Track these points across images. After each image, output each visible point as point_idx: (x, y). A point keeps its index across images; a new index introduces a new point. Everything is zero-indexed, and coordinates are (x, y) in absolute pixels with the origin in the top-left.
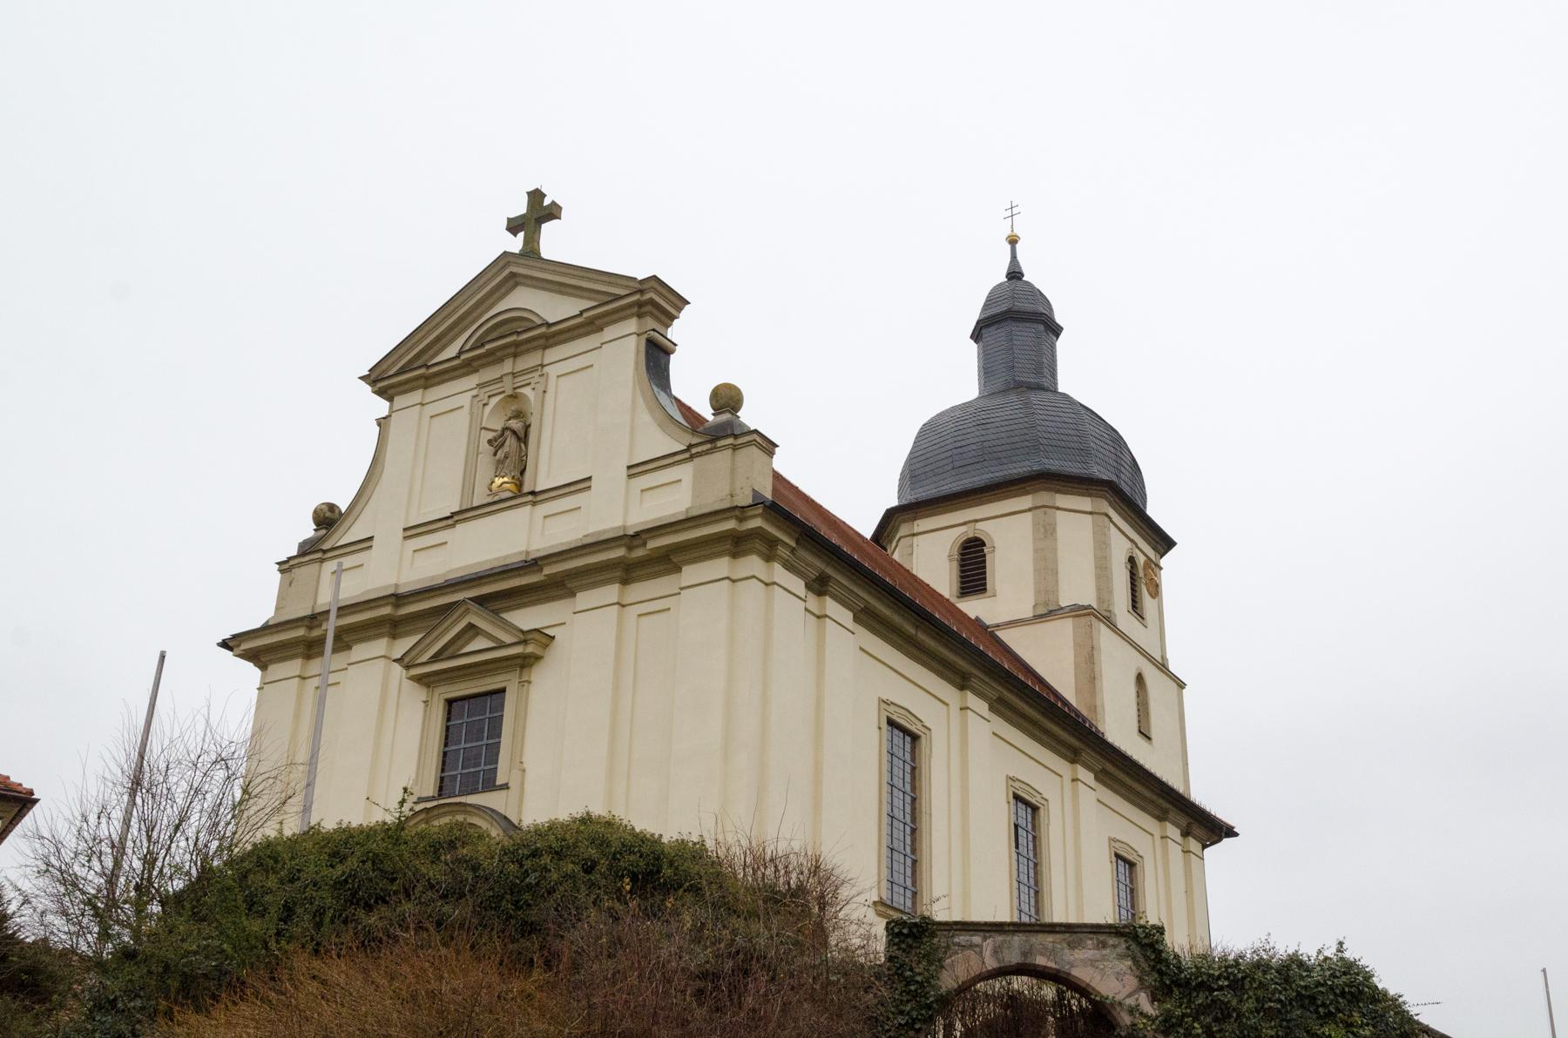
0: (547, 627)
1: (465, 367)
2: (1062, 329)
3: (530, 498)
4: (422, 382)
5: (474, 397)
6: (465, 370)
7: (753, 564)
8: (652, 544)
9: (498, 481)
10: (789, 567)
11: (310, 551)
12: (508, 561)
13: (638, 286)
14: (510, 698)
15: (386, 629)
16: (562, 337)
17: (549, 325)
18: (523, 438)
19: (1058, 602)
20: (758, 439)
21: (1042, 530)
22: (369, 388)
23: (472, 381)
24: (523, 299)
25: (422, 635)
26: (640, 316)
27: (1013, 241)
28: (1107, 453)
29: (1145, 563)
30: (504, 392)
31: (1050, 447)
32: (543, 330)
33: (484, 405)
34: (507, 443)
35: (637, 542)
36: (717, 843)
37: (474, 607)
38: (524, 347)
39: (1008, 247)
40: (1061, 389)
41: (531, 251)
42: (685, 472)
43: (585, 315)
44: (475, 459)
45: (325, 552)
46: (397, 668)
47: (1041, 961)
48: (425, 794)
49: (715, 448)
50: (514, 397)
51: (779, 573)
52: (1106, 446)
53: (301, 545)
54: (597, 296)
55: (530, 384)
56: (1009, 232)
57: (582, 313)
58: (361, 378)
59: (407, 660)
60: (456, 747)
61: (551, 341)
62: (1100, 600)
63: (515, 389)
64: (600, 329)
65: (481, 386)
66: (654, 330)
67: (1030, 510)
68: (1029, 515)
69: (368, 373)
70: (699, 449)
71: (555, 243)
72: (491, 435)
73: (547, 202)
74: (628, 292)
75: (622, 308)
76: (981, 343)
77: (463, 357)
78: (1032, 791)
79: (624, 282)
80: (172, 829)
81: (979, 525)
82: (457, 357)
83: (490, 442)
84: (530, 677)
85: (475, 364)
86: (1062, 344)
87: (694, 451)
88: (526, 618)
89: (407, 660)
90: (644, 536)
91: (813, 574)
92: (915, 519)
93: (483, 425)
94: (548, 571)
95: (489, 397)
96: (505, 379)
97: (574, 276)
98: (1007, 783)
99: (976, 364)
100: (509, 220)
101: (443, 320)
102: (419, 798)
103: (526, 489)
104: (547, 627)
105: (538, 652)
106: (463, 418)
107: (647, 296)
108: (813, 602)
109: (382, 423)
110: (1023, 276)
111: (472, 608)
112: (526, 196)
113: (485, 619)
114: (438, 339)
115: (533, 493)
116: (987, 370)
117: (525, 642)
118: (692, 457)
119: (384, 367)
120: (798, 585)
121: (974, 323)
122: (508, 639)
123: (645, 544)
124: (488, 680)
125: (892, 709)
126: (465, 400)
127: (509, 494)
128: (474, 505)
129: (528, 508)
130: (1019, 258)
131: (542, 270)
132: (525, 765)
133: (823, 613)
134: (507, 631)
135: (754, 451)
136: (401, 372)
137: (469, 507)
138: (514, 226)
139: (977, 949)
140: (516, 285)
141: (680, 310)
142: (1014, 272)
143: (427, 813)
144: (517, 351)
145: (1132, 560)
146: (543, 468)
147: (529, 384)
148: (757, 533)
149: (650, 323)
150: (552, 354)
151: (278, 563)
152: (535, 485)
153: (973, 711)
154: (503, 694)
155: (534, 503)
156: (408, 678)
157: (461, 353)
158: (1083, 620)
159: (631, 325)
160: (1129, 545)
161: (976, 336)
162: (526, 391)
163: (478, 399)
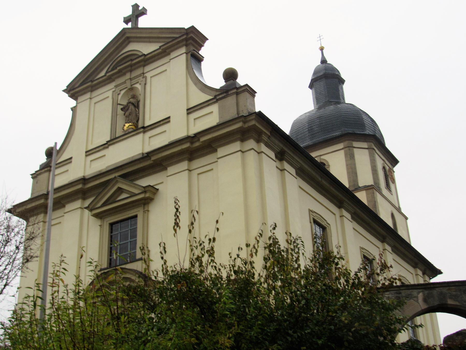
0: (156, 185)
1: (108, 80)
3: (142, 130)
4: (90, 89)
6: (108, 81)
7: (251, 144)
8: (203, 139)
9: (127, 125)
10: (267, 145)
11: (46, 167)
14: (140, 220)
15: (80, 196)
17: (145, 55)
18: (137, 106)
19: (358, 185)
20: (248, 89)
21: (349, 156)
22: (67, 95)
23: (112, 85)
24: (133, 47)
27: (322, 49)
28: (370, 126)
29: (389, 169)
32: (142, 58)
33: (119, 94)
34: (130, 108)
35: (196, 139)
37: (120, 180)
39: (320, 52)
40: (347, 102)
41: (135, 27)
43: (162, 48)
44: (116, 117)
46: (86, 211)
47: (450, 302)
48: (103, 267)
49: (229, 95)
50: (132, 89)
51: (264, 148)
52: (369, 123)
53: (41, 166)
54: (161, 40)
56: (320, 46)
57: (160, 47)
58: (64, 91)
59: (91, 207)
60: (116, 233)
61: (147, 62)
62: (375, 182)
63: (132, 85)
64: (169, 54)
65: (116, 86)
66: (194, 50)
69: (66, 88)
70: (221, 96)
71: (143, 22)
72: (122, 107)
73: (140, 8)
74: (180, 35)
75: (179, 42)
76: (313, 89)
77: (108, 75)
78: (370, 254)
81: (322, 157)
82: (105, 75)
83: (122, 109)
84: (148, 208)
85: (113, 78)
86: (345, 87)
87: (218, 97)
88: (145, 182)
89: (91, 207)
90: (198, 136)
91: (278, 150)
93: (119, 103)
94: (153, 158)
95: (120, 91)
96: (127, 82)
98: (360, 250)
99: (312, 97)
100: (124, 18)
103: (140, 125)
104: (156, 185)
105: (151, 196)
106: (110, 101)
107: (190, 36)
108: (278, 164)
109: (74, 109)
110: (327, 62)
111: (118, 180)
112: (131, 8)
113: (126, 184)
114: (96, 69)
115: (143, 127)
116: (317, 99)
117: (145, 192)
118: (217, 100)
119: (73, 84)
120: (272, 155)
121: (310, 81)
122: (136, 191)
123: (199, 140)
124: (128, 212)
125: (314, 214)
126: (110, 94)
127: (131, 130)
128: (117, 136)
130: (325, 55)
131: (141, 33)
133: (283, 168)
134: (136, 188)
135: (247, 94)
137: (114, 137)
138: (127, 21)
139: (415, 299)
140: (129, 42)
141: (204, 42)
144: (131, 68)
145: (384, 168)
146: (147, 116)
148: (254, 128)
149: (192, 48)
150: (147, 68)
151: (31, 175)
152: (144, 124)
153: (345, 217)
154: (136, 218)
155: (144, 132)
156: (92, 216)
157: (107, 72)
158: (370, 191)
159: (183, 50)
160: (382, 162)
161: (311, 86)
162: (138, 86)
163: (115, 92)
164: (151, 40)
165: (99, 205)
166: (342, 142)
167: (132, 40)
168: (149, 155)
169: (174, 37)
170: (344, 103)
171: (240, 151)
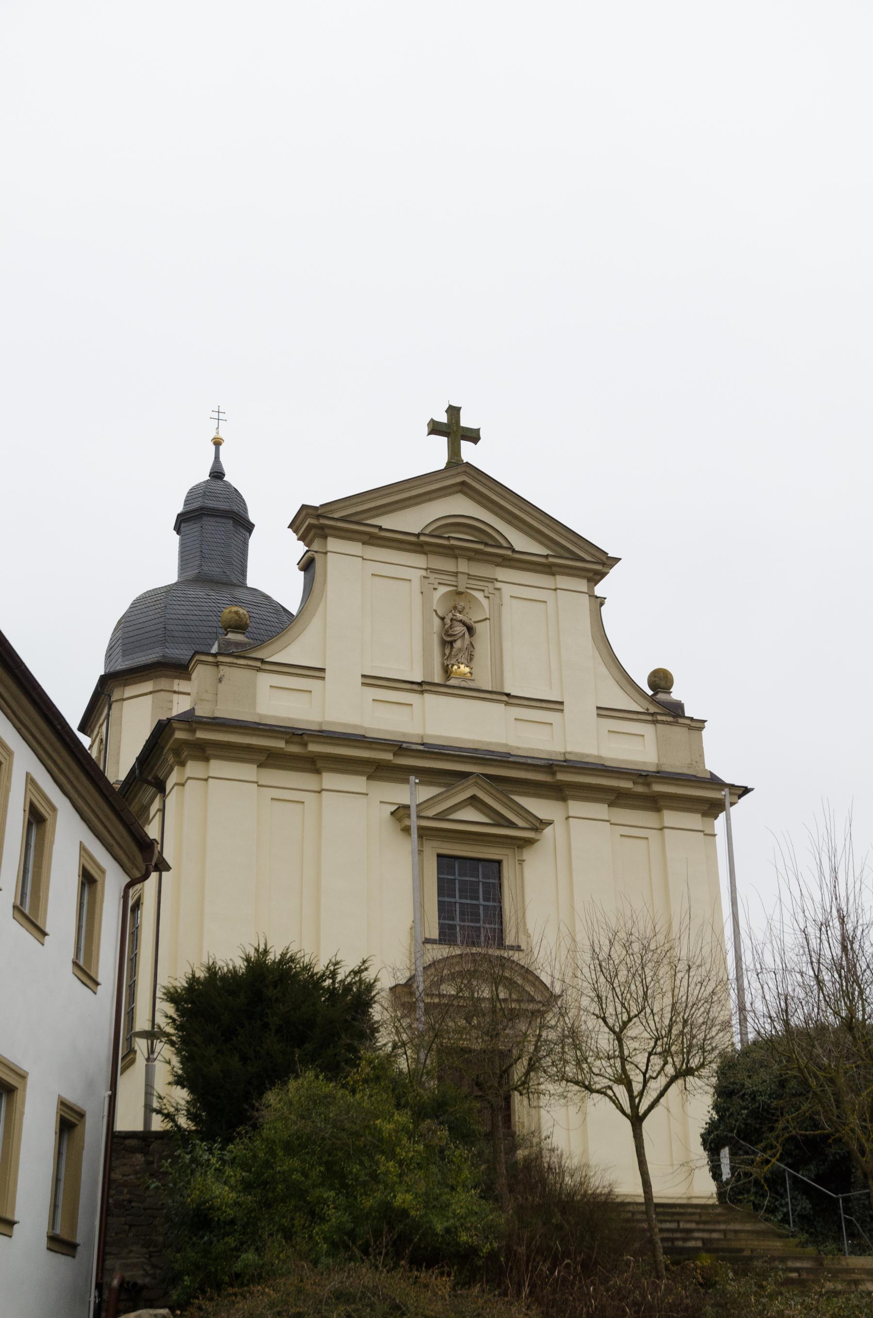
0: (728, 819)
2: (253, 526)
5: (425, 577)
13: (604, 559)
16: (517, 564)
17: (514, 551)
23: (419, 560)
27: (217, 443)
30: (456, 586)
31: (180, 639)
38: (375, 541)
39: (213, 447)
42: (648, 730)
45: (263, 661)
54: (553, 546)
55: (483, 591)
57: (547, 556)
67: (151, 693)
68: (150, 696)
77: (422, 538)
79: (593, 551)
80: (809, 965)
85: (426, 548)
92: (125, 685)
110: (224, 475)
118: (655, 722)
119: (333, 507)
124: (484, 849)
129: (502, 706)
130: (222, 459)
136: (342, 519)
142: (216, 472)
144: (475, 556)
150: (502, 573)
161: (183, 522)
163: (428, 581)
164: (515, 522)
166: (151, 679)
169: (580, 556)
170: (242, 585)
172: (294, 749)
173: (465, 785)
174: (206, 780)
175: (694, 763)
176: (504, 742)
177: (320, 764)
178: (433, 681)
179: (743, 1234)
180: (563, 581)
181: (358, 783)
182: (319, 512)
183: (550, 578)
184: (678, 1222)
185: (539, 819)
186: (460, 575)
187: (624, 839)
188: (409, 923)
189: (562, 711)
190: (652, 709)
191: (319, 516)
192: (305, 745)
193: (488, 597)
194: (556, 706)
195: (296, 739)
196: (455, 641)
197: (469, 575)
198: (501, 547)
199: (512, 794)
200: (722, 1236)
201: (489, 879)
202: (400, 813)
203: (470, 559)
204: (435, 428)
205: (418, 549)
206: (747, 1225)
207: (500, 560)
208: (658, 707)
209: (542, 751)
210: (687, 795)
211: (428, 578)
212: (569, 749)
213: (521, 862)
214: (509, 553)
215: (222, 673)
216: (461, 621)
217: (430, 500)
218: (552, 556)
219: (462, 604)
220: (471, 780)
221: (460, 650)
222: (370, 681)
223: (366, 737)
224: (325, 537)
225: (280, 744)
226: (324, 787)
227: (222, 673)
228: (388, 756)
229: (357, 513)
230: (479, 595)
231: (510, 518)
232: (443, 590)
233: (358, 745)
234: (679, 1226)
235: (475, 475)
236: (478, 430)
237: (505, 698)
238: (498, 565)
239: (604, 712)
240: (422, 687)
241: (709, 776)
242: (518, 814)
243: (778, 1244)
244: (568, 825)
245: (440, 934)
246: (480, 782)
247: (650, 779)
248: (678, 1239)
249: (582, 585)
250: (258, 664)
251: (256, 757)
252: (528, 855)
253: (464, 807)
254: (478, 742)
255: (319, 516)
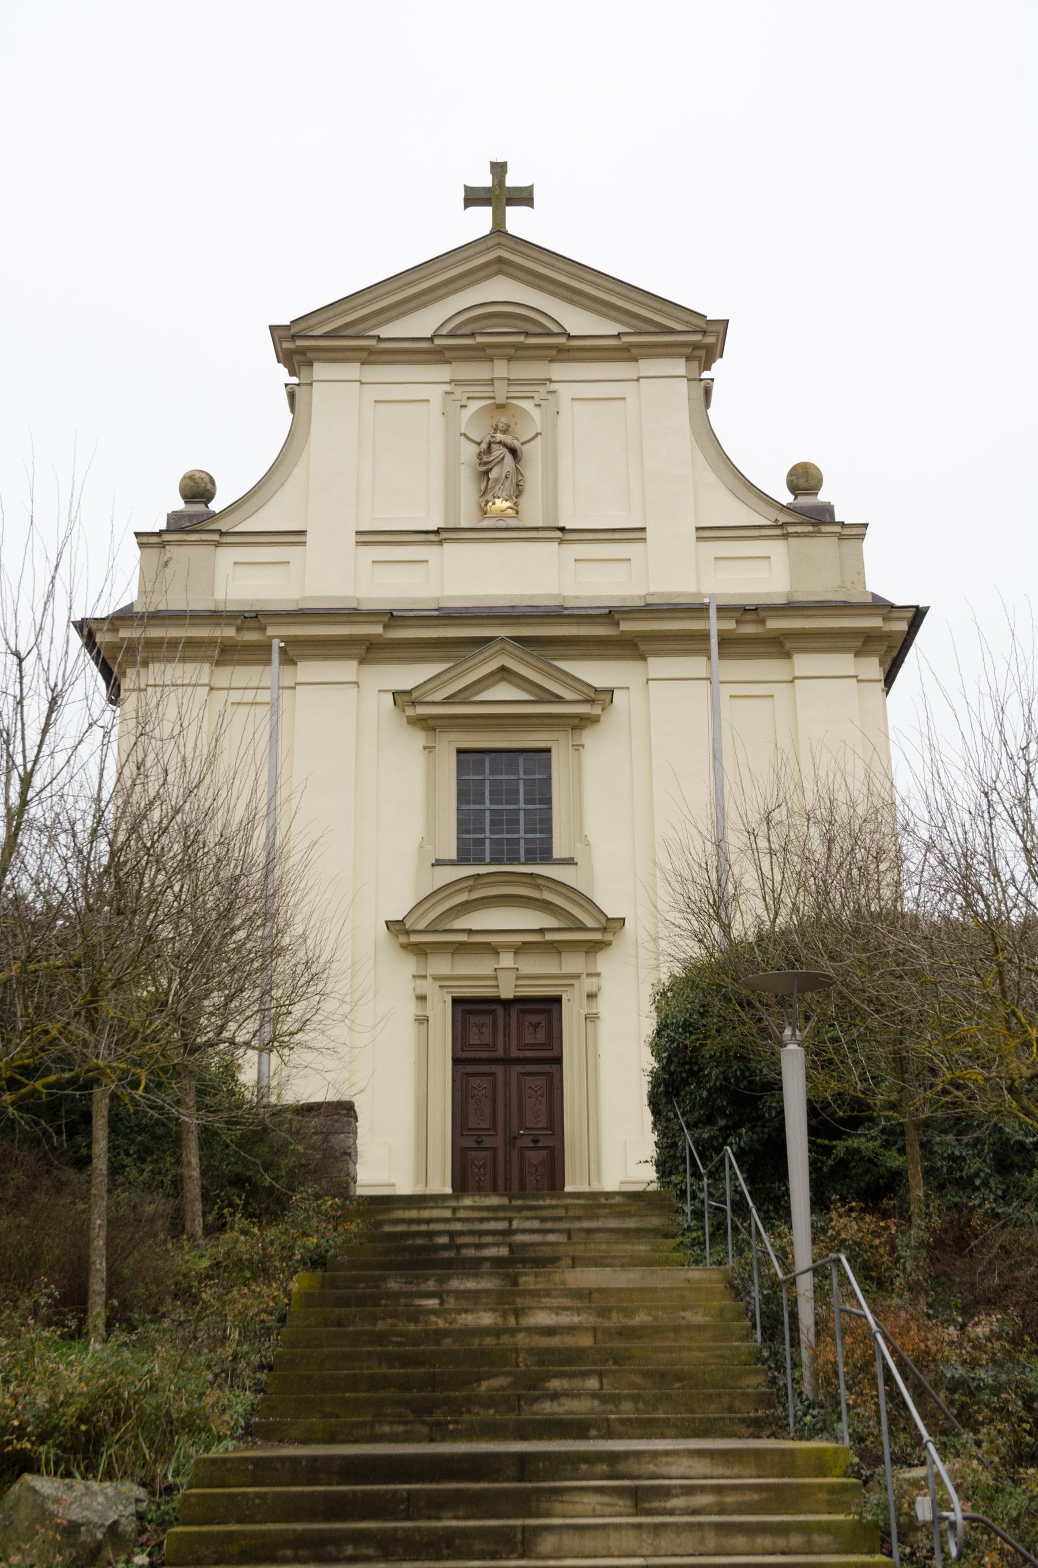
5: (447, 393)
12: (650, 600)
13: (703, 325)
15: (361, 651)
23: (443, 372)
25: (451, 664)
26: (688, 358)
30: (494, 398)
36: (304, 937)
38: (377, 358)
42: (777, 550)
45: (222, 534)
49: (819, 532)
54: (632, 321)
55: (533, 398)
57: (619, 336)
69: (289, 323)
77: (438, 342)
82: (431, 339)
85: (448, 354)
97: (611, 291)
101: (403, 286)
102: (437, 860)
117: (592, 702)
118: (786, 536)
124: (525, 736)
129: (555, 545)
132: (589, 838)
143: (476, 879)
144: (516, 353)
147: (533, 398)
150: (558, 371)
163: (452, 397)
164: (576, 298)
165: (439, 696)
167: (509, 270)
168: (617, 616)
171: (856, 677)
172: (749, 629)
173: (486, 654)
174: (792, 682)
175: (849, 585)
176: (556, 591)
177: (788, 645)
178: (457, 526)
179: (601, 1235)
180: (647, 367)
181: (346, 669)
182: (293, 331)
183: (487, 365)
184: (510, 1220)
185: (592, 687)
186: (495, 382)
187: (736, 701)
188: (418, 840)
189: (644, 540)
190: (783, 518)
191: (294, 337)
192: (763, 622)
193: (539, 405)
194: (636, 534)
195: (748, 617)
196: (491, 469)
197: (509, 380)
198: (550, 334)
199: (554, 659)
200: (565, 1240)
201: (534, 774)
202: (402, 698)
203: (510, 359)
204: (473, 198)
205: (437, 357)
206: (628, 1220)
207: (554, 353)
208: (790, 515)
209: (613, 597)
210: (312, 636)
211: (452, 393)
212: (652, 590)
213: (578, 747)
214: (562, 340)
215: (169, 555)
216: (500, 443)
217: (456, 291)
218: (625, 334)
219: (504, 420)
220: (494, 648)
221: (497, 480)
222: (367, 538)
223: (566, 608)
224: (310, 364)
225: (230, 632)
226: (797, 674)
227: (169, 555)
228: (377, 630)
229: (347, 325)
230: (527, 405)
231: (568, 294)
232: (475, 406)
233: (332, 620)
234: (510, 1224)
235: (513, 245)
236: (531, 188)
237: (559, 534)
238: (552, 360)
239: (706, 533)
240: (439, 536)
241: (869, 600)
242: (564, 684)
243: (642, 1248)
244: (648, 689)
245: (459, 851)
246: (508, 648)
247: (762, 614)
248: (467, 1246)
249: (678, 366)
250: (216, 537)
251: (849, 644)
252: (589, 737)
253: (495, 684)
254: (516, 596)
255: (294, 337)
